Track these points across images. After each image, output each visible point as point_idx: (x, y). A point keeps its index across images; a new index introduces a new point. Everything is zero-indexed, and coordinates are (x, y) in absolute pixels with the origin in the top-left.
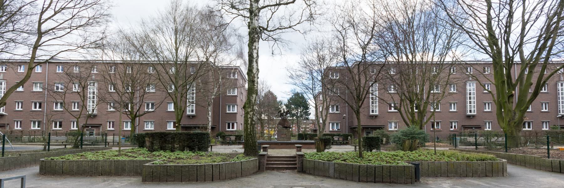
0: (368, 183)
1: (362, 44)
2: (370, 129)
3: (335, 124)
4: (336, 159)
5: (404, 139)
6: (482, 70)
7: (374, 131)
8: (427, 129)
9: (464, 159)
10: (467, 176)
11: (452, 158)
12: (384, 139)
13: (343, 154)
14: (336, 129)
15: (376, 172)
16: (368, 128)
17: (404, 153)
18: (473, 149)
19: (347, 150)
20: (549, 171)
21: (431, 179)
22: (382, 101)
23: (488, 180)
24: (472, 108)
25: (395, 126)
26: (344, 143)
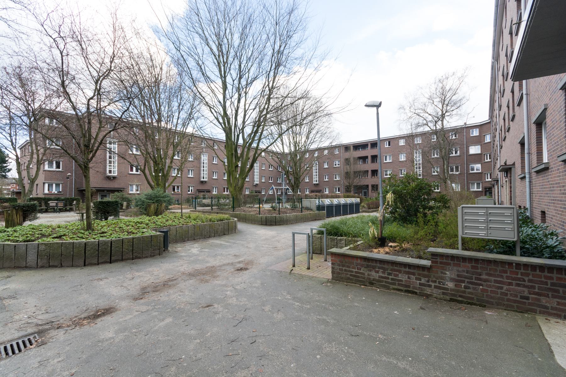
0: (100, 266)
1: (95, 74)
2: (106, 191)
3: (54, 185)
4: (43, 236)
5: (149, 202)
6: (212, 145)
7: (111, 194)
8: (169, 192)
9: (207, 221)
10: (210, 237)
11: (198, 220)
12: (125, 204)
13: (59, 227)
14: (56, 191)
15: (113, 248)
16: (103, 191)
17: (150, 218)
18: (209, 210)
19: (68, 219)
20: (260, 225)
21: (179, 245)
22: (122, 160)
23: (226, 238)
24: (205, 176)
25: (137, 189)
26: (66, 208)
